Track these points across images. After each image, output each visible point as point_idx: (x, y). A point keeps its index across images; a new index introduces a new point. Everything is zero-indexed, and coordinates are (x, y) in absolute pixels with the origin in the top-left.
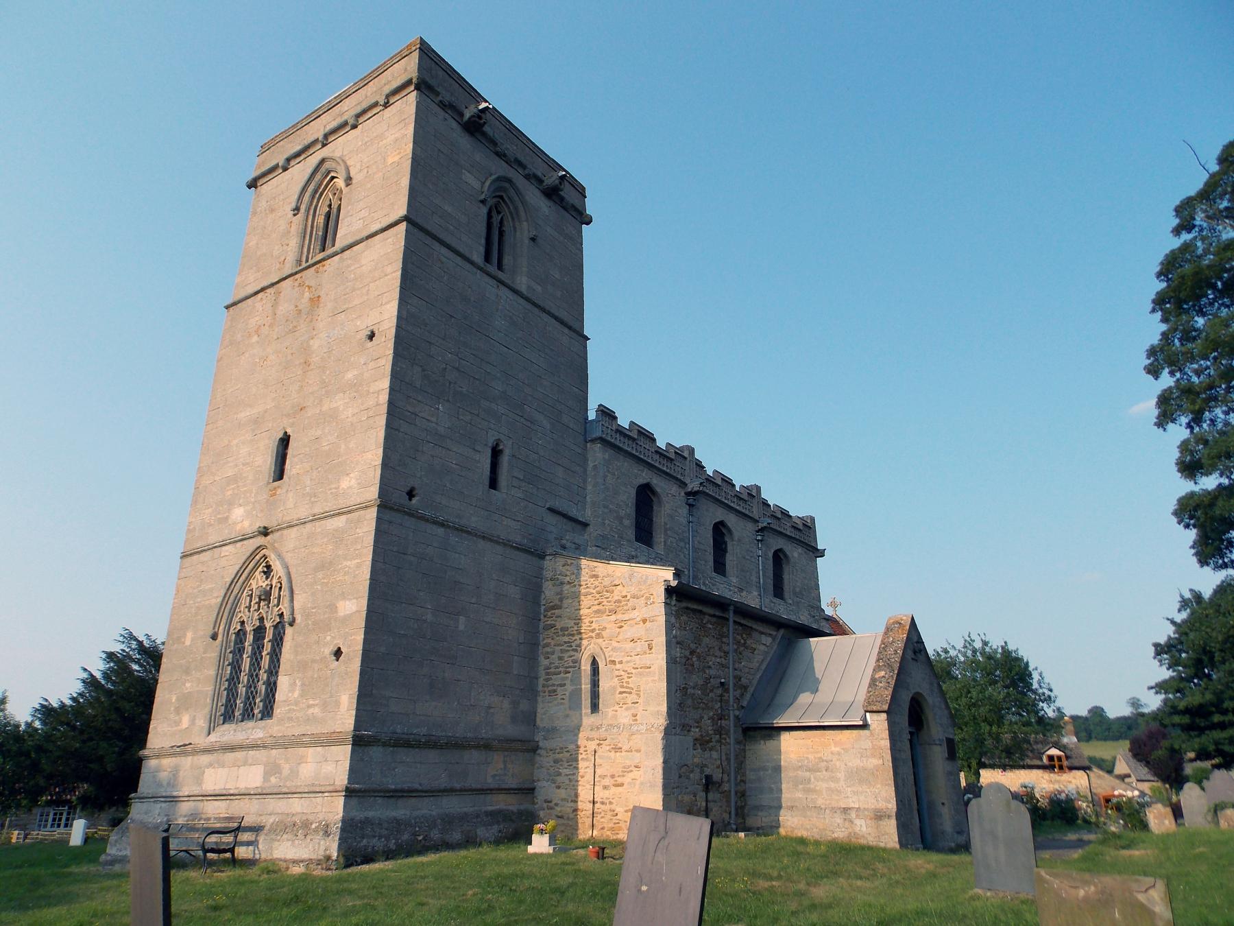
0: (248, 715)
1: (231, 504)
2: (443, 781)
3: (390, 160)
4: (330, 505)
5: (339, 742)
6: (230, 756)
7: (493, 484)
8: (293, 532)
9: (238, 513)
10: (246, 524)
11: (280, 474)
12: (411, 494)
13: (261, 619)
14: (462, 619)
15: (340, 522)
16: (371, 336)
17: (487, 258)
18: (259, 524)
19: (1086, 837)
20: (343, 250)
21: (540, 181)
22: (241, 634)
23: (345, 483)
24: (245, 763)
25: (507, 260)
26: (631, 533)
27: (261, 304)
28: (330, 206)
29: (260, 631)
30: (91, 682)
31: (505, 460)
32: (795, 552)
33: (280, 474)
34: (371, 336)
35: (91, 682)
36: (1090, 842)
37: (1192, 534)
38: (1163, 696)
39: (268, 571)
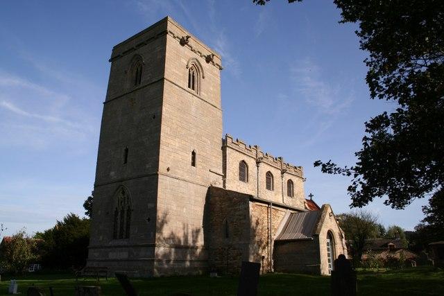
0: (121, 237)
3: (158, 57)
5: (95, 248)
7: (193, 164)
8: (131, 181)
9: (112, 173)
10: (115, 177)
12: (168, 170)
14: (185, 209)
15: (147, 178)
17: (189, 87)
19: (344, 240)
20: (143, 87)
22: (116, 212)
25: (196, 86)
26: (238, 178)
30: (59, 224)
31: (197, 156)
35: (59, 224)
36: (342, 240)
37: (386, 228)
39: (123, 193)
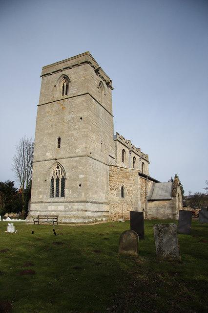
0: (57, 196)
1: (46, 152)
2: (97, 210)
4: (74, 155)
6: (55, 204)
9: (48, 154)
11: (59, 147)
13: (58, 177)
16: (81, 119)
18: (54, 157)
21: (105, 81)
22: (52, 180)
23: (77, 150)
24: (59, 205)
27: (48, 106)
28: (63, 85)
29: (58, 180)
32: (145, 162)
33: (59, 147)
34: (81, 119)
38: (8, 231)
